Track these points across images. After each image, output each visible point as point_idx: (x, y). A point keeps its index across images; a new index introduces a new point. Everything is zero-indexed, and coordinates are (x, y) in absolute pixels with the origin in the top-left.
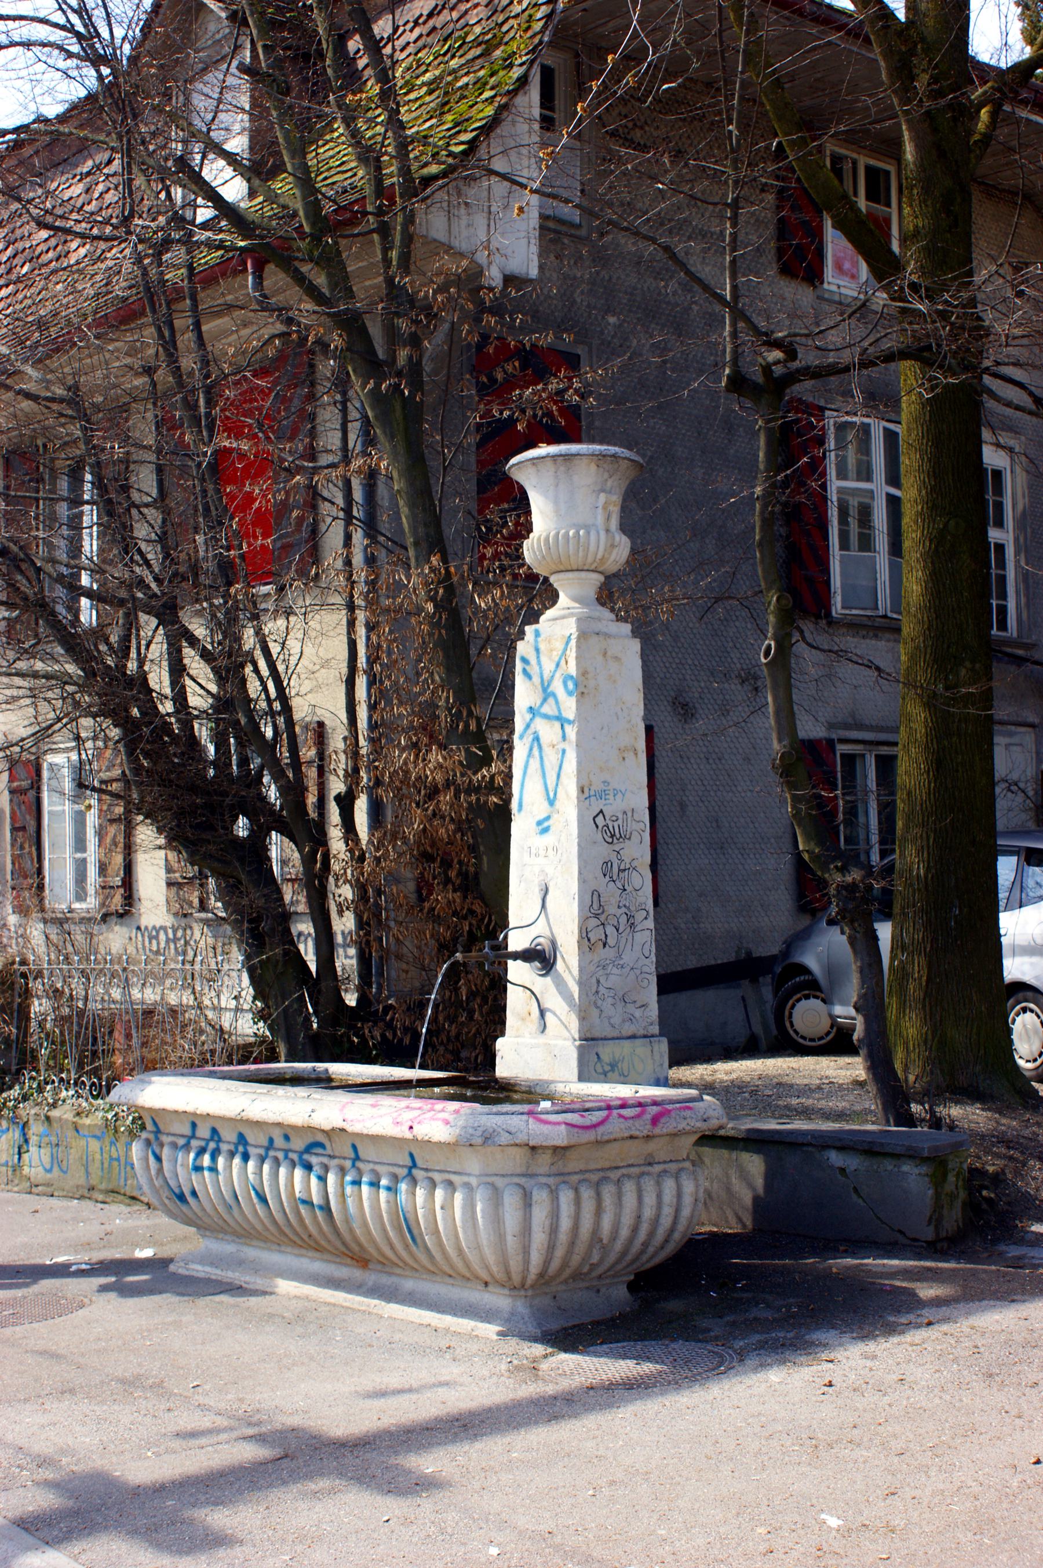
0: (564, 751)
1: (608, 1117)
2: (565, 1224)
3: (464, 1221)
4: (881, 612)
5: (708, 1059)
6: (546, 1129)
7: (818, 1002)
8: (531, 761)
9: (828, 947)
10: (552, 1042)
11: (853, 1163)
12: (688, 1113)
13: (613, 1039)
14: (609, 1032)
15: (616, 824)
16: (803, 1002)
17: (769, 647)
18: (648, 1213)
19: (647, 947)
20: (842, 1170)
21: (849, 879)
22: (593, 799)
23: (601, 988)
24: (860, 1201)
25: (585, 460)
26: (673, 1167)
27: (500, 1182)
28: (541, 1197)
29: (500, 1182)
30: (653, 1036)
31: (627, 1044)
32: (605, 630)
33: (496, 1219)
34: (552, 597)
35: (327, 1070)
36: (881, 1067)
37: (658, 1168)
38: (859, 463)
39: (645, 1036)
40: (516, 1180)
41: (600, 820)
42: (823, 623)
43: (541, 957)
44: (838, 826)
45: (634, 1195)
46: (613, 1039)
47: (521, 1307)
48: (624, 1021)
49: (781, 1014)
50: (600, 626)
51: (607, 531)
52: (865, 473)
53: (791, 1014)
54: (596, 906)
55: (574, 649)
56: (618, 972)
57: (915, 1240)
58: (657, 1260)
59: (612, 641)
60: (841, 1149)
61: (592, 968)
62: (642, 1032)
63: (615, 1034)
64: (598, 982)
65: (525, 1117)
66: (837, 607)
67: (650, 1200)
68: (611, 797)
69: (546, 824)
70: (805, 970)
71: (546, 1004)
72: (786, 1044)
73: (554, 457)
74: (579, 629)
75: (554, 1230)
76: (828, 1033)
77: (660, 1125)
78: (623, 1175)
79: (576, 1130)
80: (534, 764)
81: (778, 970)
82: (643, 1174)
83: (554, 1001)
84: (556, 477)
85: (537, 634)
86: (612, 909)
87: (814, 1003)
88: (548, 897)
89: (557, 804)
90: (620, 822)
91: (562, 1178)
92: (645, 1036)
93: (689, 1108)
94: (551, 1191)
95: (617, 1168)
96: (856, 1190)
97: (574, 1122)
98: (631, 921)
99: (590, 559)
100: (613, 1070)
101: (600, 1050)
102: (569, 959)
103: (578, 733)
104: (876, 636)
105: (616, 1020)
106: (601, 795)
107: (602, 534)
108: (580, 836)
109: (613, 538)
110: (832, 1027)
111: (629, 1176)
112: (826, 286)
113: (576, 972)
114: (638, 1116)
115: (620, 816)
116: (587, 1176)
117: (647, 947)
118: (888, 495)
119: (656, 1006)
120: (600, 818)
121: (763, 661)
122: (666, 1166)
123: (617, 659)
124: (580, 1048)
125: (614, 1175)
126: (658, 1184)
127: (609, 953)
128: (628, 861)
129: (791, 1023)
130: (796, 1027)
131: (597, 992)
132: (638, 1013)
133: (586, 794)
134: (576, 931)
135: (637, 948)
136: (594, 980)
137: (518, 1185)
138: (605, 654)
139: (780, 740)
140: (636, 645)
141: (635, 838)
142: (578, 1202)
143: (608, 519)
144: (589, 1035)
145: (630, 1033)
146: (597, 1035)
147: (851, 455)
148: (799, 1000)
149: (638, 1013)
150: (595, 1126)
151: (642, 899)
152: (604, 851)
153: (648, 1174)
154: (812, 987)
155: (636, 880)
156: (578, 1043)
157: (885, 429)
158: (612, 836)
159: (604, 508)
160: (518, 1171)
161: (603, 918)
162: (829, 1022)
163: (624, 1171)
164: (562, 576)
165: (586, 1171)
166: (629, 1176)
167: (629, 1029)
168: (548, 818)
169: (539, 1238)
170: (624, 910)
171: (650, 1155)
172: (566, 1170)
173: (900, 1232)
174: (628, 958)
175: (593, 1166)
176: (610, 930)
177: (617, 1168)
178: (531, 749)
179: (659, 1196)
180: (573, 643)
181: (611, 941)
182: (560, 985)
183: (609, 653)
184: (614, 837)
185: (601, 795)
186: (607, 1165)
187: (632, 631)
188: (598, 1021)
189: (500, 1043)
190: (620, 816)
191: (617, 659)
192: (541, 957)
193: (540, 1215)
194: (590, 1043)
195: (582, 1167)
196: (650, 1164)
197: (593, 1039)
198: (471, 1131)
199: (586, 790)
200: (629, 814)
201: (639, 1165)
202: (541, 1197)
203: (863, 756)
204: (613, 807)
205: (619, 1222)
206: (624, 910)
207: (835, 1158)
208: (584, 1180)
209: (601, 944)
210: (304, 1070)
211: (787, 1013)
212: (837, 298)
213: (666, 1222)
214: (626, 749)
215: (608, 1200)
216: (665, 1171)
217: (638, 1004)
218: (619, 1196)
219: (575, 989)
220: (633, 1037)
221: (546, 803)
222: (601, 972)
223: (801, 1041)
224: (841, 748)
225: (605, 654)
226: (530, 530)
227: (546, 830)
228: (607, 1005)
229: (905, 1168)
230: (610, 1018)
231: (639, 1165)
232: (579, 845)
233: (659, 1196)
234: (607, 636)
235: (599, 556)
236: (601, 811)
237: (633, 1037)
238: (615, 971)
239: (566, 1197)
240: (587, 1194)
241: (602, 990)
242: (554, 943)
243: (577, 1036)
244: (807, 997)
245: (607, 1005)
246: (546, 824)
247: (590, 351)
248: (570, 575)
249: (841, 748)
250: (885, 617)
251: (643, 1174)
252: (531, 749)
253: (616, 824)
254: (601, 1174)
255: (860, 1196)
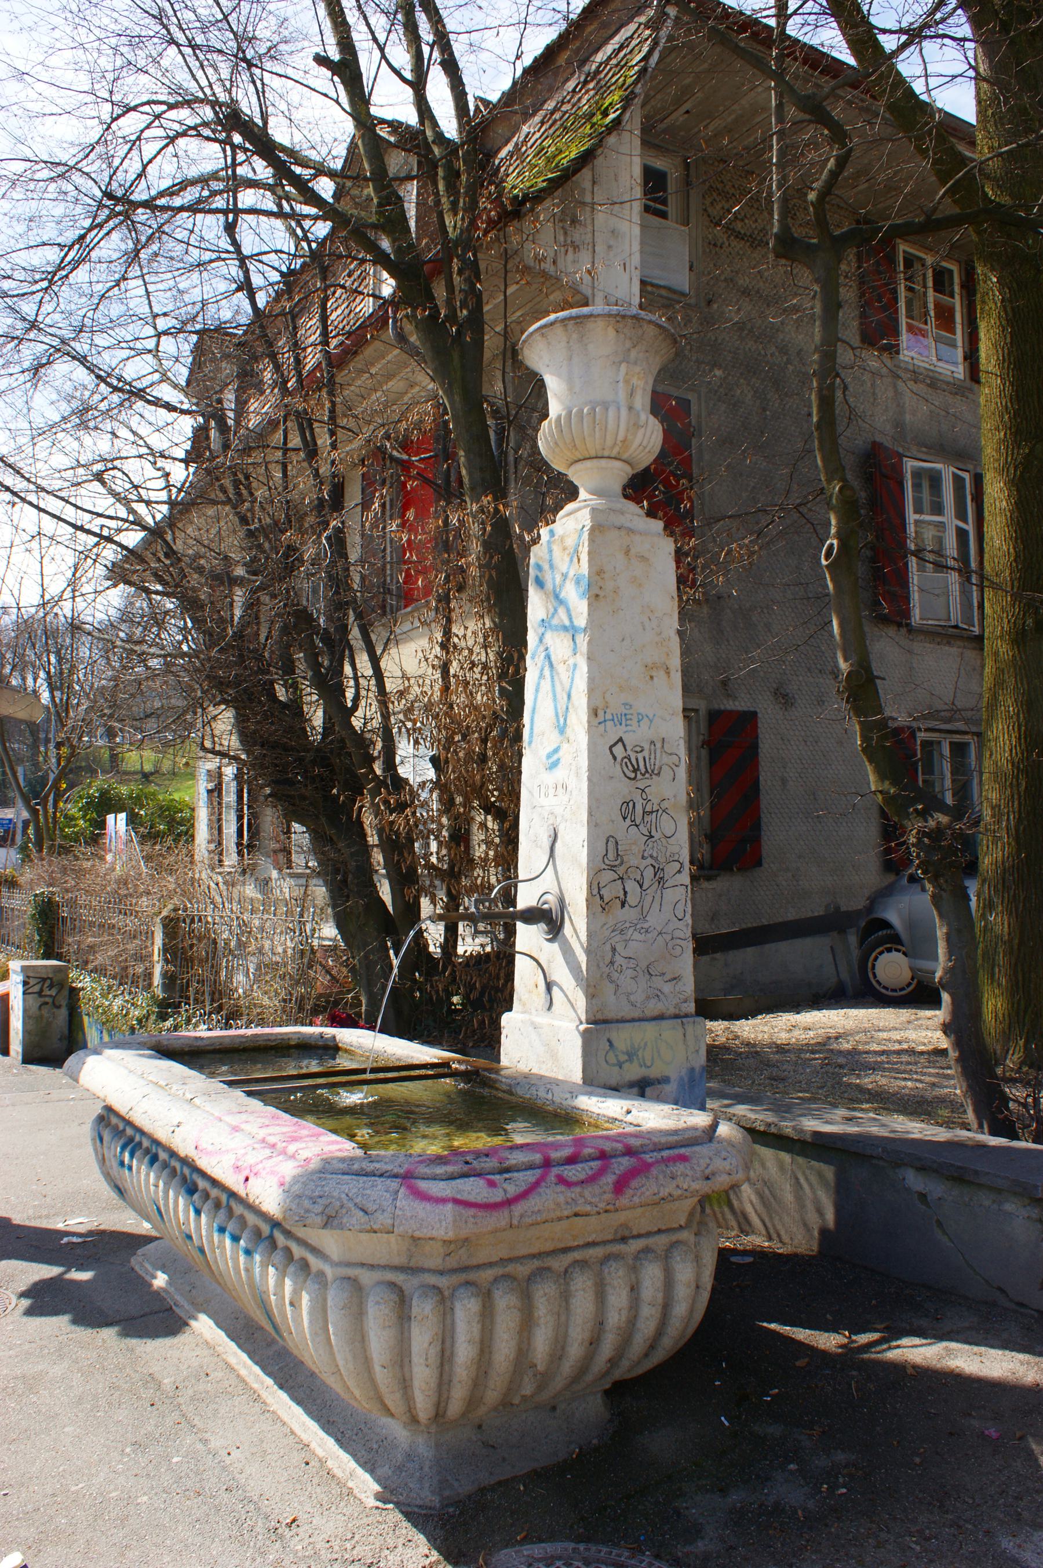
0: (575, 665)
1: (536, 1184)
2: (464, 1352)
3: (314, 1334)
4: (953, 623)
5: (797, 1007)
6: (422, 1209)
7: (900, 954)
8: (542, 682)
9: (913, 906)
10: (556, 1023)
11: (936, 1189)
12: (680, 1168)
13: (633, 1020)
14: (627, 1012)
15: (640, 756)
16: (885, 955)
17: (831, 546)
18: (615, 1318)
19: (680, 907)
20: (923, 1197)
21: (932, 823)
22: (609, 724)
23: (617, 958)
24: (945, 1239)
25: (600, 323)
26: (661, 1241)
27: (367, 1277)
28: (423, 1308)
29: (367, 1277)
30: (686, 1016)
31: (650, 1028)
32: (628, 525)
33: (359, 1337)
34: (572, 493)
35: (334, 1037)
36: (963, 1028)
37: (635, 1245)
38: (932, 502)
39: (676, 1016)
40: (390, 1276)
41: (619, 750)
42: (903, 630)
43: (550, 919)
44: (916, 762)
45: (590, 1296)
46: (633, 1020)
47: (424, 1447)
48: (648, 998)
49: (864, 967)
50: (621, 520)
51: (630, 408)
52: (938, 508)
53: (874, 966)
54: (611, 855)
55: (586, 544)
56: (642, 937)
57: (1021, 1305)
58: (640, 1371)
59: (637, 538)
60: (922, 1169)
61: (607, 933)
62: (672, 1011)
63: (636, 1014)
64: (614, 950)
65: (394, 1184)
66: (916, 617)
67: (618, 1300)
68: (634, 722)
69: (555, 757)
70: (886, 925)
71: (554, 977)
72: (867, 993)
73: (563, 320)
74: (593, 519)
75: (445, 1358)
76: (909, 984)
77: (629, 1192)
78: (576, 1262)
79: (472, 1211)
80: (546, 685)
81: (863, 924)
82: (607, 1258)
83: (562, 974)
84: (569, 349)
85: (552, 533)
86: (634, 860)
87: (896, 956)
88: (558, 845)
89: (569, 731)
90: (646, 753)
91: (463, 1277)
92: (676, 1016)
93: (683, 1158)
94: (443, 1300)
95: (566, 1250)
96: (940, 1224)
97: (471, 1198)
98: (660, 874)
99: (609, 442)
100: (630, 1060)
101: (613, 1036)
102: (577, 923)
103: (590, 643)
104: (949, 643)
105: (638, 997)
106: (621, 719)
107: (624, 412)
108: (590, 769)
109: (638, 415)
110: (913, 979)
111: (583, 1264)
112: (901, 357)
113: (584, 938)
114: (592, 1179)
115: (646, 746)
116: (510, 1268)
117: (680, 907)
118: (957, 527)
119: (692, 979)
120: (619, 750)
121: (824, 562)
122: (650, 1241)
123: (643, 559)
124: (586, 1035)
125: (558, 1264)
126: (634, 1269)
127: (628, 914)
128: (656, 801)
129: (874, 975)
130: (879, 977)
131: (612, 963)
132: (667, 988)
133: (601, 718)
134: (585, 887)
135: (667, 908)
136: (608, 947)
137: (392, 1285)
138: (627, 552)
139: (846, 660)
140: (668, 546)
141: (666, 773)
142: (487, 1315)
143: (632, 394)
144: (599, 1016)
145: (656, 1013)
146: (611, 1015)
147: (926, 495)
148: (881, 953)
149: (667, 988)
150: (509, 1202)
151: (675, 849)
152: (624, 788)
153: (617, 1257)
154: (893, 941)
155: (666, 825)
156: (582, 1027)
157: (954, 474)
158: (635, 771)
159: (627, 382)
160: (396, 1261)
161: (621, 871)
162: (909, 975)
163: (577, 1255)
164: (579, 466)
165: (510, 1260)
166: (583, 1264)
167: (654, 1007)
168: (556, 750)
169: (422, 1375)
170: (650, 861)
171: (625, 1226)
172: (474, 1262)
173: (1000, 1289)
174: (654, 920)
175: (523, 1251)
176: (631, 886)
177: (566, 1250)
178: (542, 670)
179: (634, 1289)
180: (586, 535)
181: (632, 900)
182: (567, 952)
183: (633, 551)
184: (637, 770)
185: (621, 719)
186: (549, 1246)
187: (665, 528)
188: (612, 998)
189: (506, 1019)
190: (646, 746)
191: (643, 559)
192: (550, 919)
193: (422, 1339)
194: (599, 1026)
195: (504, 1254)
196: (624, 1239)
197: (605, 1022)
198: (307, 1203)
199: (601, 713)
200: (659, 745)
201: (604, 1243)
202: (423, 1308)
203: (939, 743)
204: (637, 735)
205: (566, 1335)
206: (650, 861)
207: (914, 1180)
208: (506, 1277)
209: (618, 903)
210: (311, 1035)
211: (870, 965)
212: (911, 367)
213: (647, 1326)
214: (654, 666)
215: (542, 1308)
216: (647, 1250)
217: (668, 977)
218: (566, 1296)
219: (582, 958)
220: (661, 1017)
221: (556, 731)
222: (618, 938)
223: (883, 991)
224: (921, 736)
225: (627, 552)
226: (546, 415)
227: (555, 765)
228: (625, 979)
229: (1008, 1207)
230: (628, 994)
231: (604, 1243)
232: (589, 779)
233: (634, 1289)
234: (630, 531)
235: (621, 437)
236: (621, 740)
237: (661, 1017)
238: (637, 936)
239: (466, 1312)
240: (505, 1302)
241: (619, 960)
242: (561, 901)
243: (583, 1018)
244: (889, 950)
245: (625, 979)
246: (555, 757)
247: (699, 398)
248: (588, 464)
249: (921, 736)
250: (956, 627)
251: (607, 1258)
252: (542, 670)
253: (640, 756)
254: (537, 1263)
255: (945, 1233)
